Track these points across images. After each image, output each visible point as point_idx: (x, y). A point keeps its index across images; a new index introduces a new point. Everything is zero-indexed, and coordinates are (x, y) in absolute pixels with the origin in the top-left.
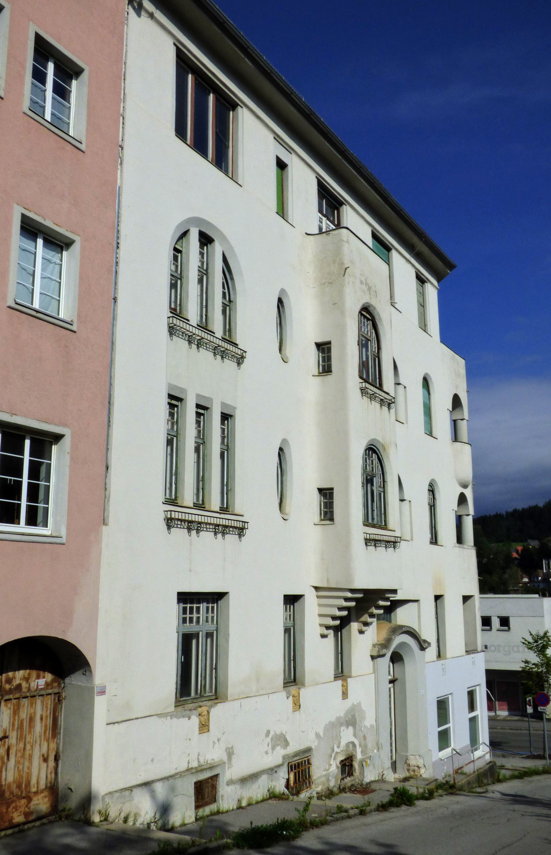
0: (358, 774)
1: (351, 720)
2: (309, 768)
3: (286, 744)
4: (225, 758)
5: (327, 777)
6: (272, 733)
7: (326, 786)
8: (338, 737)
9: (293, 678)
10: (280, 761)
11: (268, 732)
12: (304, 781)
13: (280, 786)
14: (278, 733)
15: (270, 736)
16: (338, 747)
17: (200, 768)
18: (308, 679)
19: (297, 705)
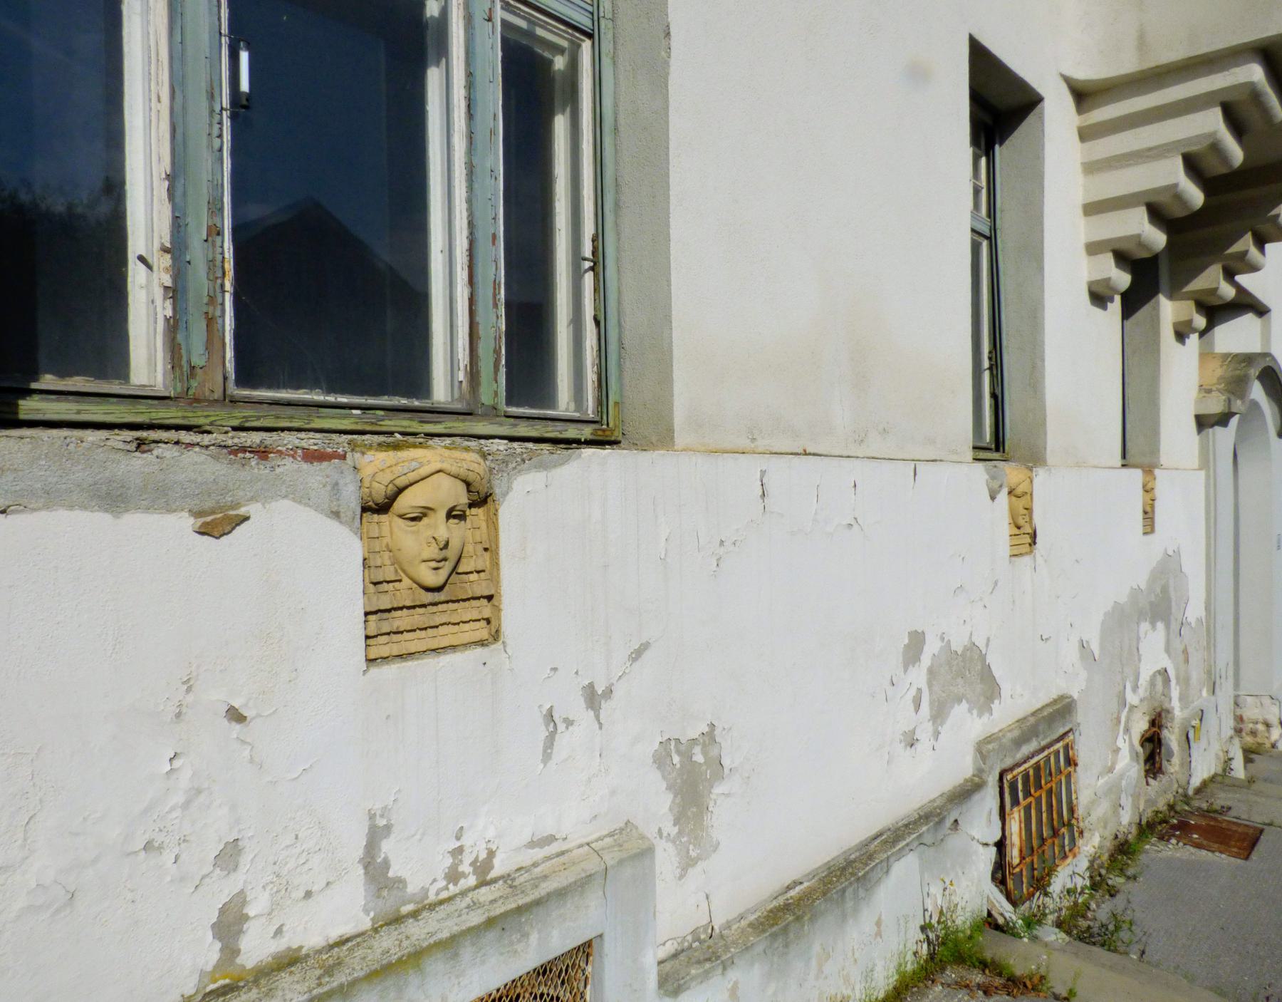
0: (1177, 768)
1: (1158, 604)
2: (1069, 776)
3: (990, 689)
4: (654, 805)
5: (1114, 791)
6: (932, 647)
7: (1109, 834)
8: (1134, 654)
9: (999, 435)
10: (962, 767)
11: (917, 640)
12: (1055, 833)
13: (971, 890)
14: (957, 646)
15: (926, 660)
16: (1135, 688)
17: (388, 944)
18: (1054, 441)
19: (1026, 536)
